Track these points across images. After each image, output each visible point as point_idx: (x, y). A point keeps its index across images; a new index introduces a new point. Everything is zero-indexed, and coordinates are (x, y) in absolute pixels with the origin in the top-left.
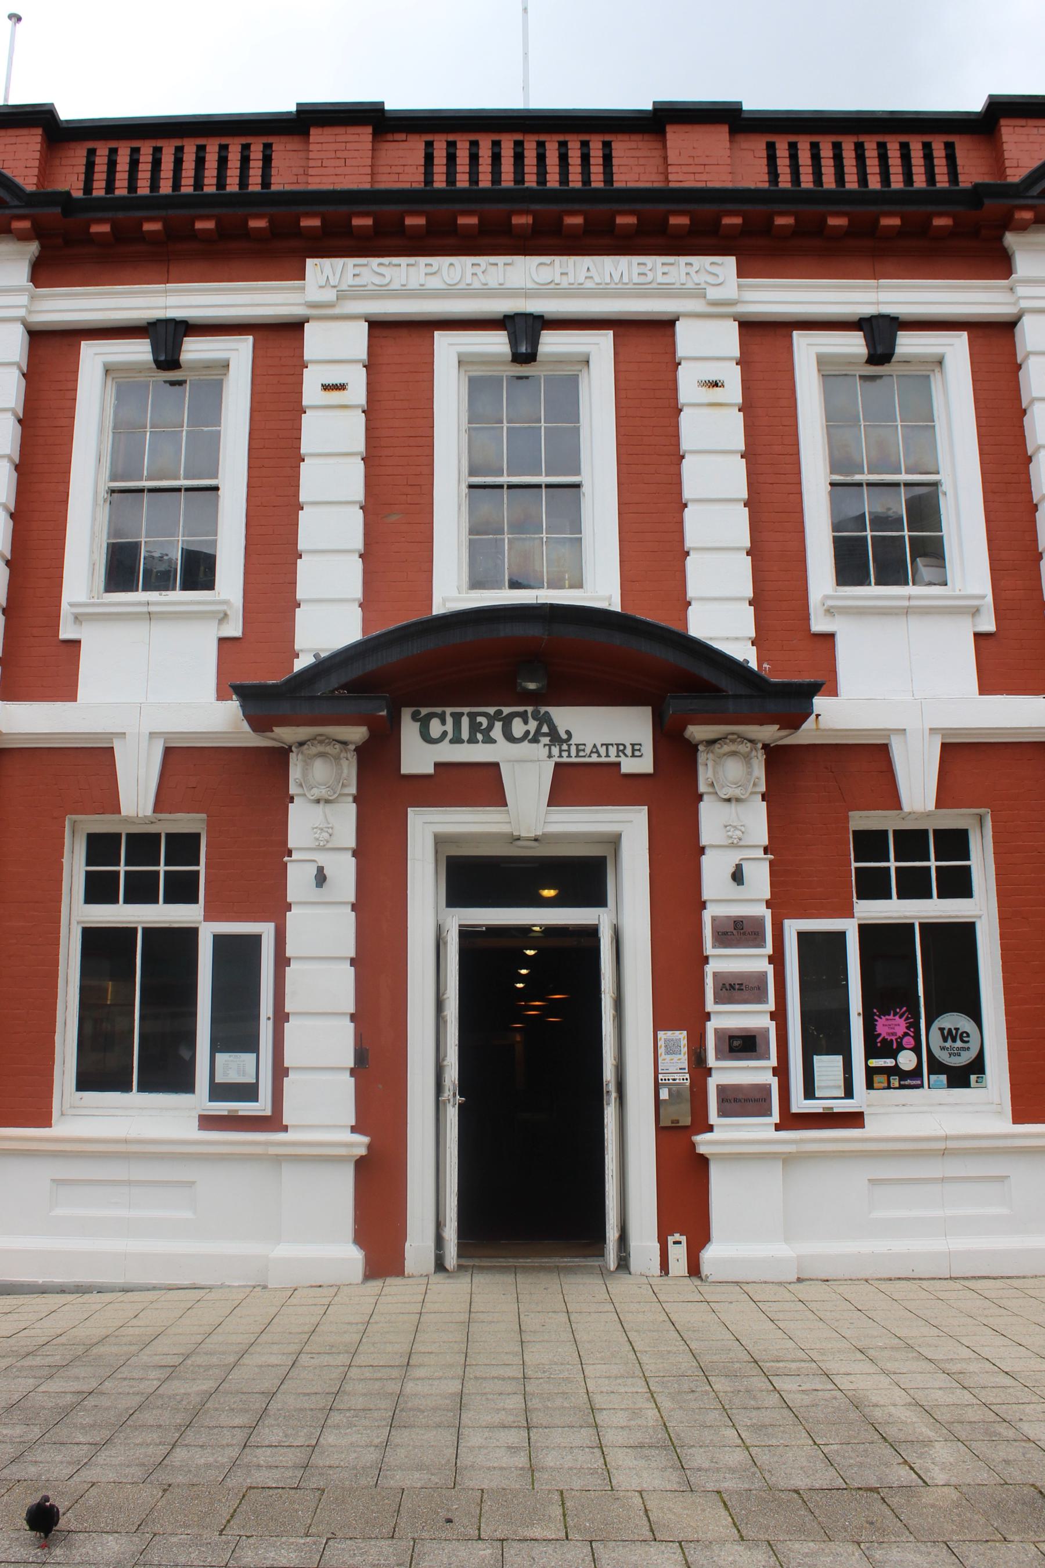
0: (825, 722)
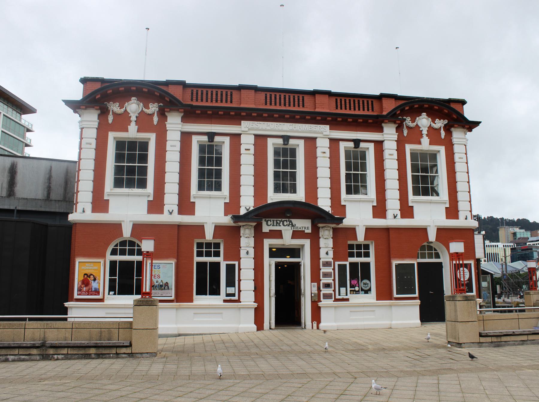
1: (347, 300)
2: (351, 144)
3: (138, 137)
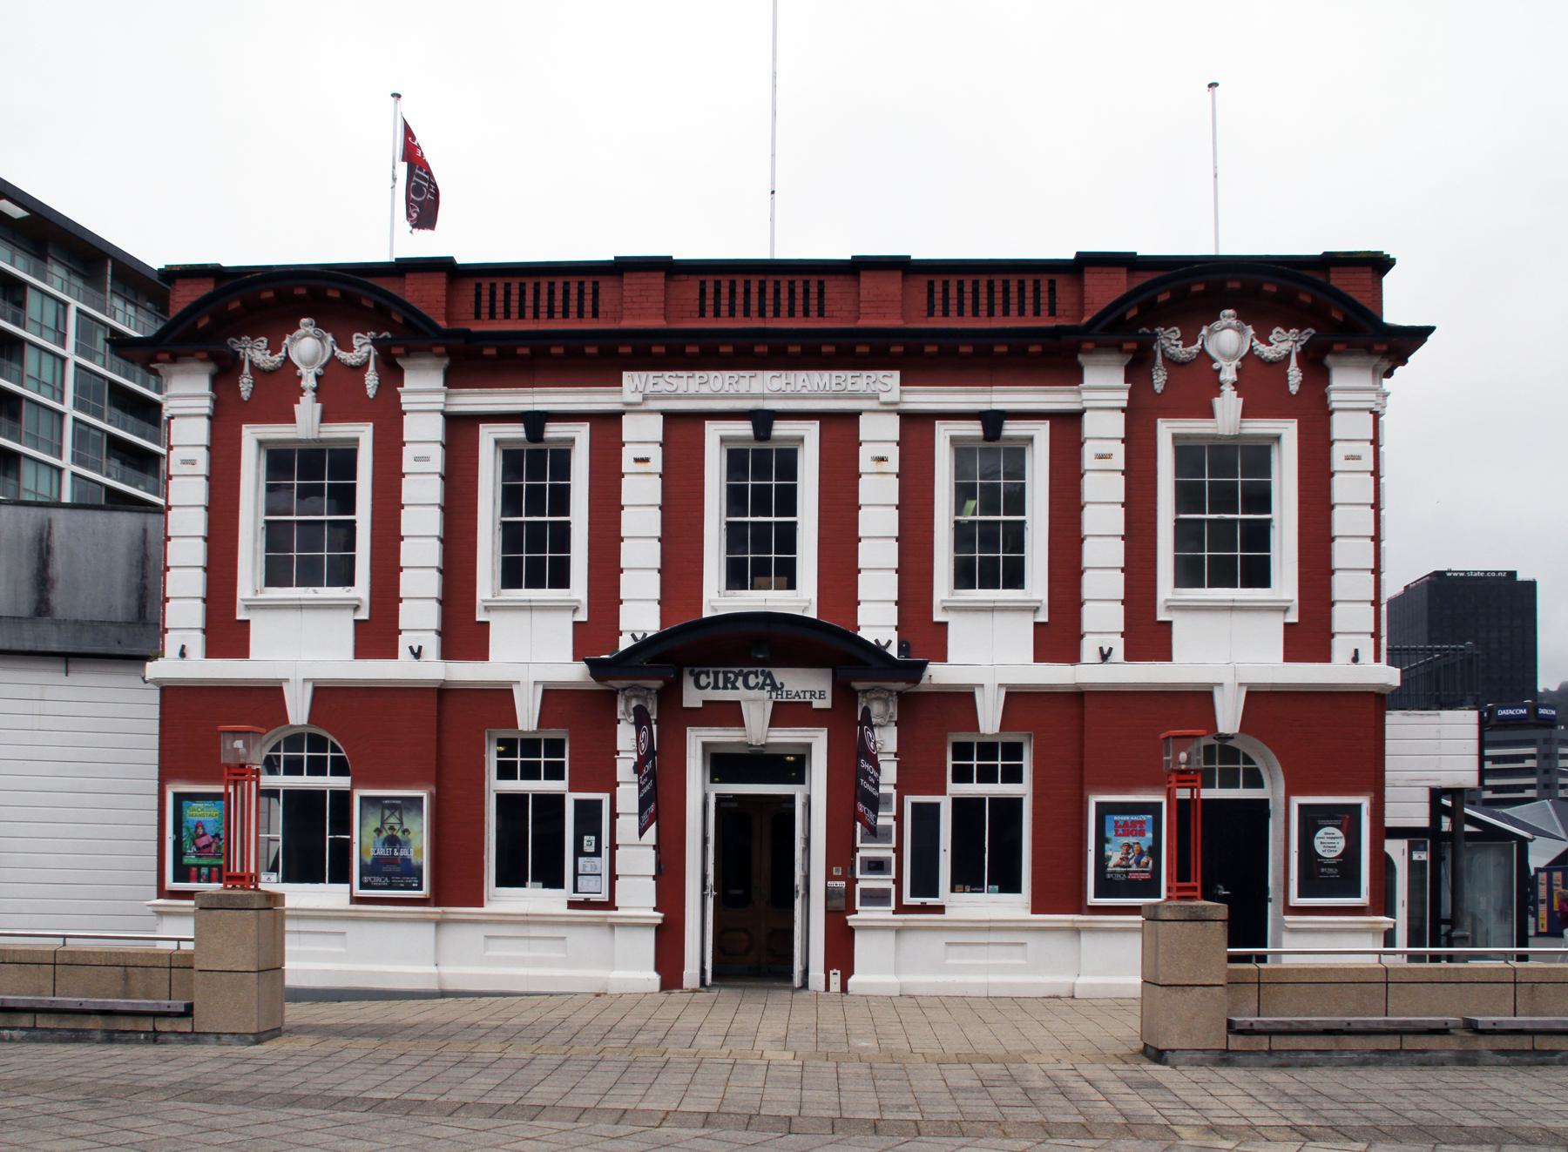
0: (935, 680)
1: (940, 909)
2: (974, 429)
3: (323, 436)
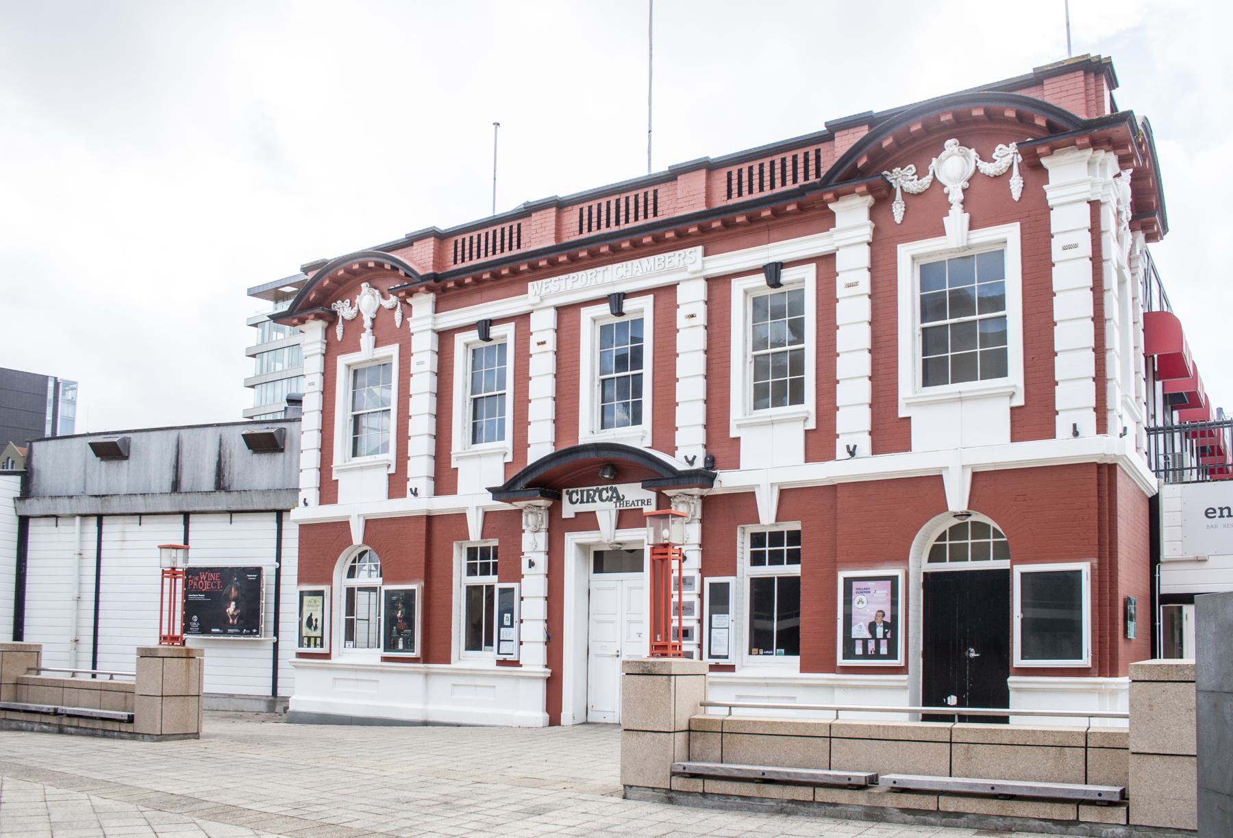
0: (725, 484)
2: (760, 280)
